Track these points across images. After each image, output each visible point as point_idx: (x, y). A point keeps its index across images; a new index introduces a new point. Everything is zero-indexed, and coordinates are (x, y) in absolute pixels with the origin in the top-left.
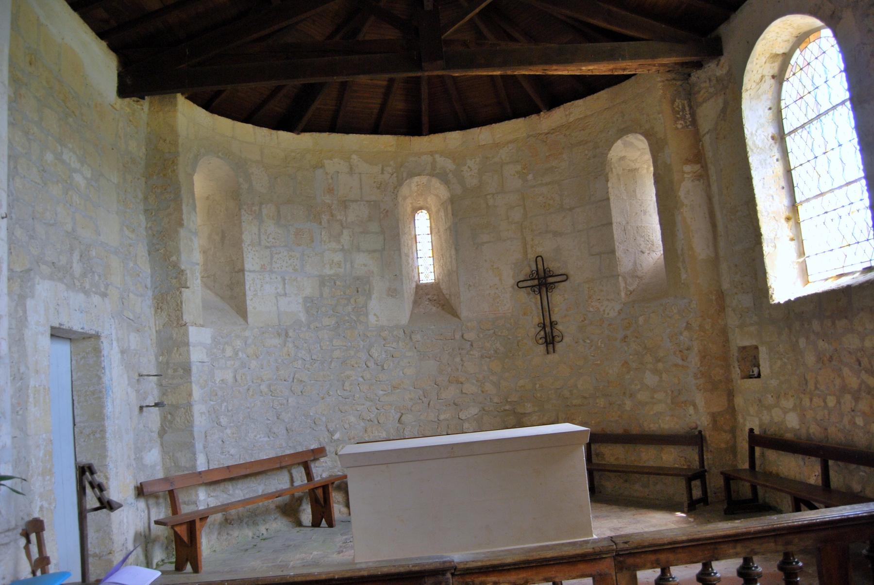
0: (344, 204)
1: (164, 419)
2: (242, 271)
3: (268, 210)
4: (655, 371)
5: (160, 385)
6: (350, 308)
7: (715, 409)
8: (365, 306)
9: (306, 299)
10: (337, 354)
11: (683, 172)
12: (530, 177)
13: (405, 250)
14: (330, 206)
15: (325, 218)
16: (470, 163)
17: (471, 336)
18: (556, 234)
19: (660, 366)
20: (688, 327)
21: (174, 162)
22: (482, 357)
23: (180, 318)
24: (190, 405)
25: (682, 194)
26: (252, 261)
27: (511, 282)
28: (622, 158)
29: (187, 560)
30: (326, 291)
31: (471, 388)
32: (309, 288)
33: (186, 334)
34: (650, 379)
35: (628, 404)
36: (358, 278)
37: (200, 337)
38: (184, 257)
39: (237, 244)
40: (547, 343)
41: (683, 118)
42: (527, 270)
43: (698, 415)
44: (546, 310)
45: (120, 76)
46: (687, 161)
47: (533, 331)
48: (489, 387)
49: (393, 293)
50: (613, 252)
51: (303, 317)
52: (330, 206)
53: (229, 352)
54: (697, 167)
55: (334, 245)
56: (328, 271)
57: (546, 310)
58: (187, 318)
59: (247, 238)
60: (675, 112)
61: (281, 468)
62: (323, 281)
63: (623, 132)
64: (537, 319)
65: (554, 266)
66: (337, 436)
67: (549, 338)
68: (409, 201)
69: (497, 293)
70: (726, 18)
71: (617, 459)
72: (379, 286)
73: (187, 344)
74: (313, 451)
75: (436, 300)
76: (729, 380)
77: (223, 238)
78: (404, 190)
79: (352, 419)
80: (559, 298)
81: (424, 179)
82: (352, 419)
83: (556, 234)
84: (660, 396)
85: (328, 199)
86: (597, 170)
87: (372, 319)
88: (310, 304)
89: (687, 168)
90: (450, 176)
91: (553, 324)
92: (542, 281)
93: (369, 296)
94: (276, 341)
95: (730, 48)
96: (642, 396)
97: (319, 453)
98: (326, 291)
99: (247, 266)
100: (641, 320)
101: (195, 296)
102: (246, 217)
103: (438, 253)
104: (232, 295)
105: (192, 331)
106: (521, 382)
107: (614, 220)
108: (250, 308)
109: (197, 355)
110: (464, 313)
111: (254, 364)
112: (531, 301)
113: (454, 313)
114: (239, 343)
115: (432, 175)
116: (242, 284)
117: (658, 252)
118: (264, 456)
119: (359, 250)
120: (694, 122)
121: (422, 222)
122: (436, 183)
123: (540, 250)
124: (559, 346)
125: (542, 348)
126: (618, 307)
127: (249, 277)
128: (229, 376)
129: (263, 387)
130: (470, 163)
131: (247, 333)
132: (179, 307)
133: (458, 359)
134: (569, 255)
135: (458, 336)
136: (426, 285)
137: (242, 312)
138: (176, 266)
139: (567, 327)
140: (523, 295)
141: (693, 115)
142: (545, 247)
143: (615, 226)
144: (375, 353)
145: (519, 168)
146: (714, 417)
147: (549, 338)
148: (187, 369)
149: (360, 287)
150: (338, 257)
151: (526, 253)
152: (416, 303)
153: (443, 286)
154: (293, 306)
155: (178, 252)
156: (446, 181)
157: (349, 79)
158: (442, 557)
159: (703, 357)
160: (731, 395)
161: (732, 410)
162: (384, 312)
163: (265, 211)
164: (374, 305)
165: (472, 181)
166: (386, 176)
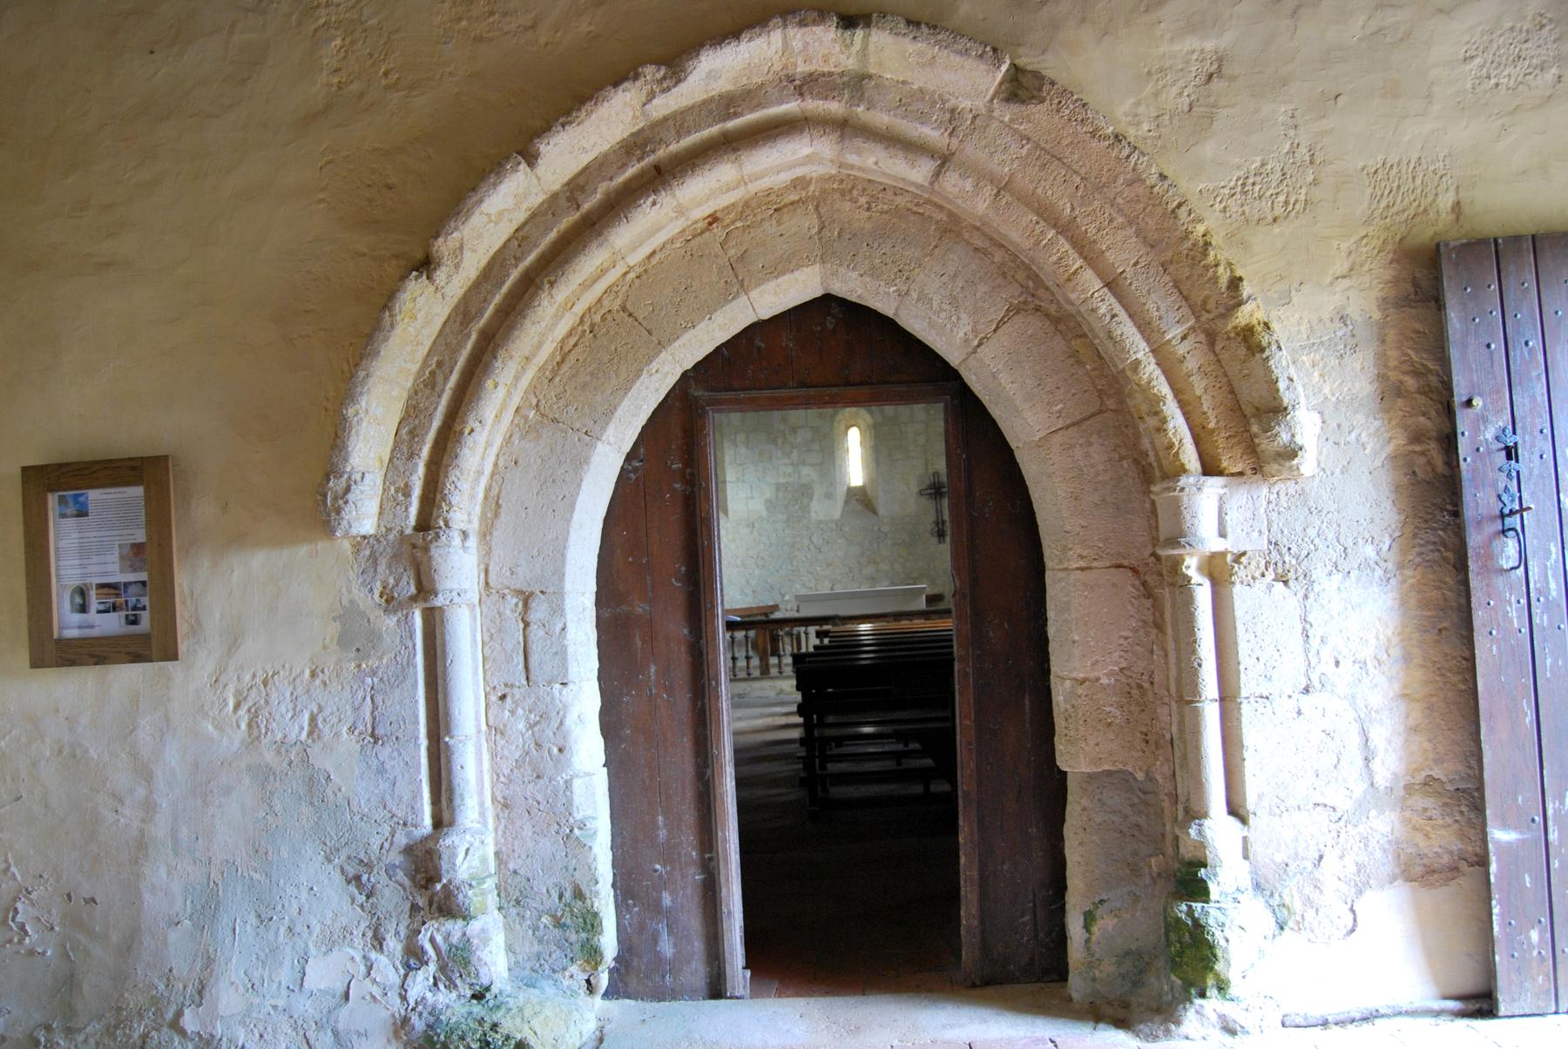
13: (838, 463)
15: (780, 441)
17: (885, 528)
27: (916, 490)
31: (884, 567)
32: (769, 493)
42: (927, 482)
47: (929, 528)
48: (897, 567)
49: (829, 496)
51: (764, 513)
55: (786, 461)
56: (782, 480)
59: (727, 459)
62: (778, 487)
64: (933, 518)
71: (784, 420)
72: (818, 490)
75: (861, 500)
87: (813, 515)
88: (770, 505)
94: (747, 531)
102: (726, 444)
110: (881, 511)
113: (875, 512)
119: (804, 464)
127: (729, 486)
149: (805, 491)
150: (790, 470)
152: (847, 502)
154: (758, 506)
157: (948, 539)
158: (196, 628)
162: (825, 509)
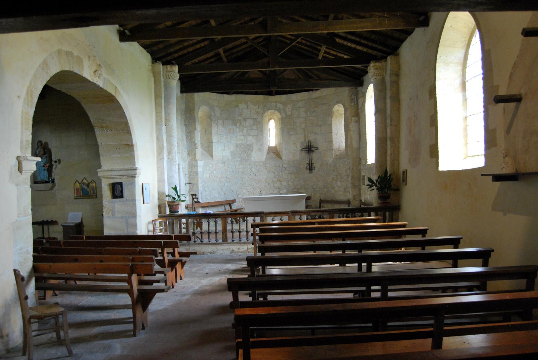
0: (245, 119)
1: (190, 188)
2: (212, 142)
3: (220, 122)
4: (340, 181)
5: (189, 178)
6: (245, 155)
7: (355, 194)
8: (251, 154)
9: (231, 152)
10: (241, 170)
11: (352, 120)
12: (308, 113)
13: (265, 135)
14: (240, 120)
15: (238, 124)
16: (289, 106)
18: (316, 134)
19: (342, 180)
20: (349, 169)
21: (194, 110)
22: (289, 173)
23: (195, 158)
24: (198, 184)
25: (351, 127)
26: (215, 139)
28: (338, 110)
29: (25, 349)
30: (238, 149)
31: (284, 183)
32: (232, 148)
33: (197, 163)
34: (339, 184)
35: (333, 191)
36: (248, 145)
37: (200, 163)
38: (196, 139)
39: (210, 134)
40: (310, 170)
41: (354, 102)
42: (305, 145)
43: (349, 196)
44: (310, 159)
45: (181, 87)
46: (353, 116)
47: (305, 166)
48: (290, 183)
49: (260, 150)
50: (332, 142)
51: (230, 158)
52: (240, 120)
53: (208, 169)
54: (356, 118)
55: (241, 133)
56: (238, 142)
57: (310, 159)
58: (197, 158)
59: (213, 131)
60: (351, 100)
61: (222, 205)
62: (237, 146)
63: (337, 102)
64: (307, 162)
65: (314, 144)
66: (240, 196)
67: (311, 168)
68: (267, 117)
69: (293, 152)
70: (365, 75)
73: (197, 166)
74: (232, 200)
75: (275, 152)
76: (360, 185)
77: (206, 131)
78: (266, 114)
79: (245, 191)
80: (315, 155)
81: (272, 111)
82: (245, 191)
83: (316, 134)
84: (341, 189)
85: (239, 118)
86: (329, 114)
87: (253, 159)
88: (233, 154)
89: (353, 118)
90: (282, 111)
91: (312, 164)
92: (310, 149)
93: (252, 151)
94: (222, 165)
95: (365, 84)
96: (336, 189)
97: (234, 201)
98: (238, 149)
99: (214, 141)
100: (338, 165)
101: (199, 151)
102: (213, 125)
103: (277, 136)
104: (209, 150)
105: (199, 162)
106: (301, 182)
107: (333, 131)
108: (214, 155)
109: (200, 169)
110: (283, 158)
111: (215, 172)
112: (306, 155)
113: (281, 158)
114: (211, 166)
115: (275, 110)
116: (211, 146)
117: (343, 145)
118: (217, 201)
119: (249, 135)
120: (357, 103)
121: (272, 123)
122: (277, 112)
123: (310, 138)
124: (313, 171)
125: (308, 171)
126: (332, 160)
127: (214, 144)
128: (208, 176)
129: (218, 180)
130: (289, 106)
131: (213, 162)
132: (195, 155)
133: (281, 174)
134: (319, 142)
135: (281, 166)
136: (272, 147)
137: (212, 156)
138: (194, 142)
139: (317, 165)
140: (303, 153)
141: (357, 101)
142: (311, 138)
143: (333, 133)
144: (253, 170)
145: (305, 110)
146: (354, 196)
147: (311, 168)
148: (197, 174)
149: (249, 148)
150: (242, 138)
151: (305, 139)
152: (268, 153)
153: (278, 148)
154: (227, 154)
155: (194, 137)
156: (280, 113)
159: (352, 178)
160: (360, 190)
161: (360, 194)
162: (259, 156)
163: (219, 123)
164: (254, 154)
165: (289, 113)
166: (260, 110)
